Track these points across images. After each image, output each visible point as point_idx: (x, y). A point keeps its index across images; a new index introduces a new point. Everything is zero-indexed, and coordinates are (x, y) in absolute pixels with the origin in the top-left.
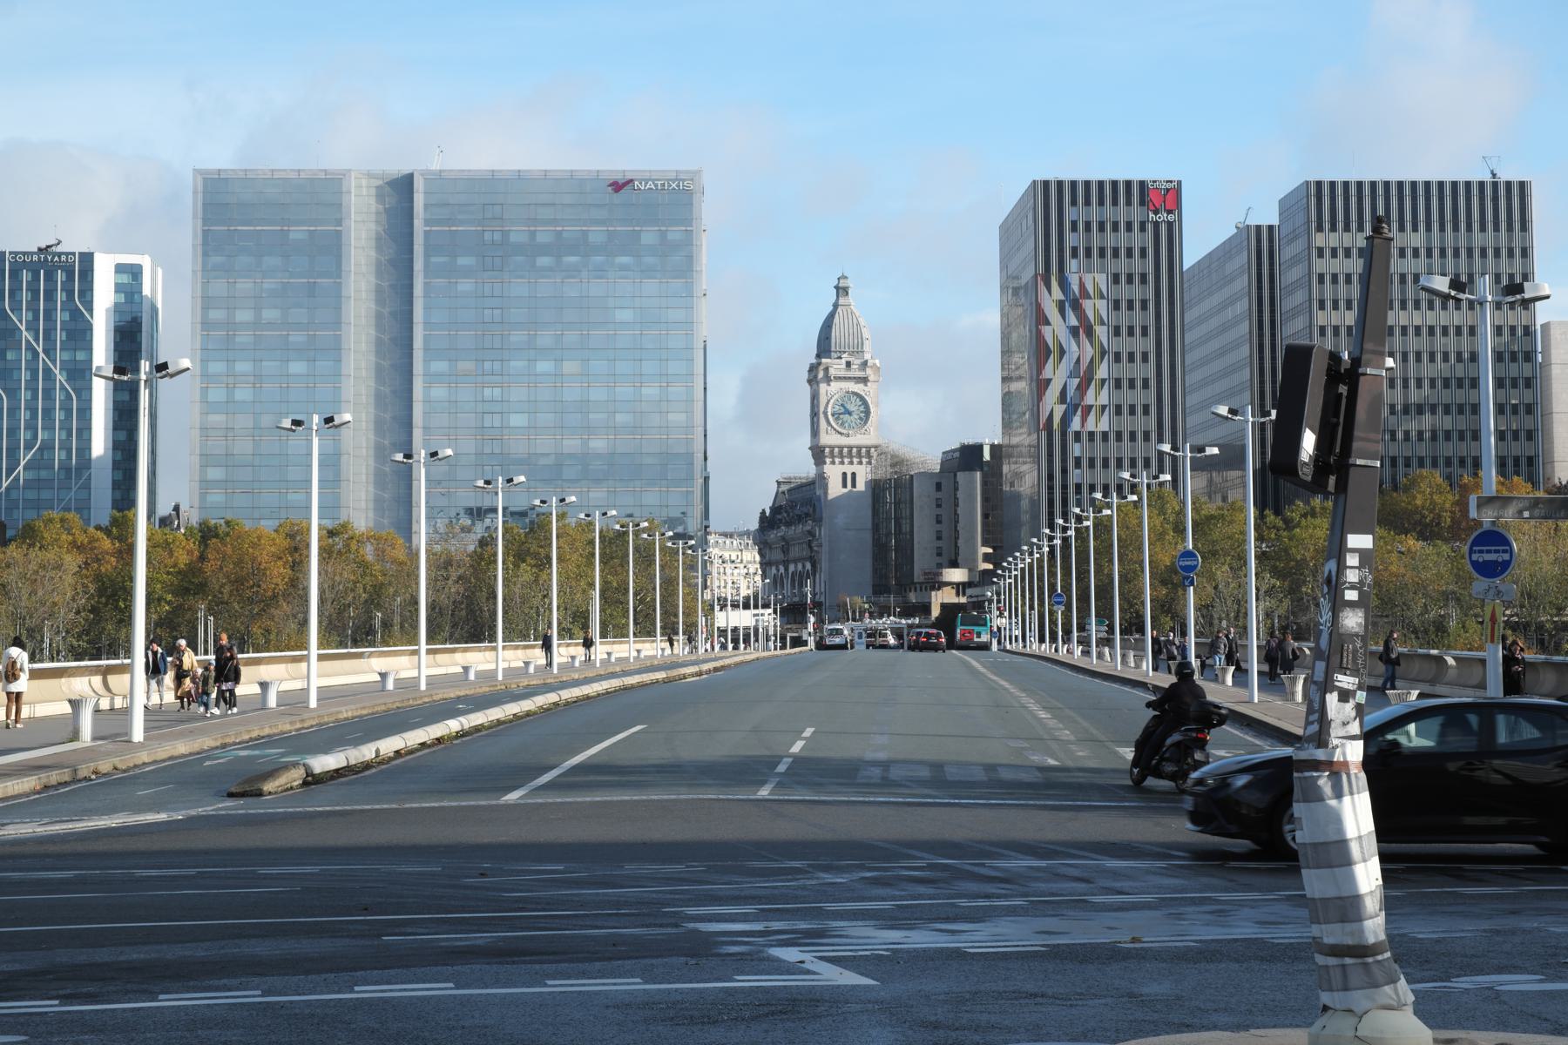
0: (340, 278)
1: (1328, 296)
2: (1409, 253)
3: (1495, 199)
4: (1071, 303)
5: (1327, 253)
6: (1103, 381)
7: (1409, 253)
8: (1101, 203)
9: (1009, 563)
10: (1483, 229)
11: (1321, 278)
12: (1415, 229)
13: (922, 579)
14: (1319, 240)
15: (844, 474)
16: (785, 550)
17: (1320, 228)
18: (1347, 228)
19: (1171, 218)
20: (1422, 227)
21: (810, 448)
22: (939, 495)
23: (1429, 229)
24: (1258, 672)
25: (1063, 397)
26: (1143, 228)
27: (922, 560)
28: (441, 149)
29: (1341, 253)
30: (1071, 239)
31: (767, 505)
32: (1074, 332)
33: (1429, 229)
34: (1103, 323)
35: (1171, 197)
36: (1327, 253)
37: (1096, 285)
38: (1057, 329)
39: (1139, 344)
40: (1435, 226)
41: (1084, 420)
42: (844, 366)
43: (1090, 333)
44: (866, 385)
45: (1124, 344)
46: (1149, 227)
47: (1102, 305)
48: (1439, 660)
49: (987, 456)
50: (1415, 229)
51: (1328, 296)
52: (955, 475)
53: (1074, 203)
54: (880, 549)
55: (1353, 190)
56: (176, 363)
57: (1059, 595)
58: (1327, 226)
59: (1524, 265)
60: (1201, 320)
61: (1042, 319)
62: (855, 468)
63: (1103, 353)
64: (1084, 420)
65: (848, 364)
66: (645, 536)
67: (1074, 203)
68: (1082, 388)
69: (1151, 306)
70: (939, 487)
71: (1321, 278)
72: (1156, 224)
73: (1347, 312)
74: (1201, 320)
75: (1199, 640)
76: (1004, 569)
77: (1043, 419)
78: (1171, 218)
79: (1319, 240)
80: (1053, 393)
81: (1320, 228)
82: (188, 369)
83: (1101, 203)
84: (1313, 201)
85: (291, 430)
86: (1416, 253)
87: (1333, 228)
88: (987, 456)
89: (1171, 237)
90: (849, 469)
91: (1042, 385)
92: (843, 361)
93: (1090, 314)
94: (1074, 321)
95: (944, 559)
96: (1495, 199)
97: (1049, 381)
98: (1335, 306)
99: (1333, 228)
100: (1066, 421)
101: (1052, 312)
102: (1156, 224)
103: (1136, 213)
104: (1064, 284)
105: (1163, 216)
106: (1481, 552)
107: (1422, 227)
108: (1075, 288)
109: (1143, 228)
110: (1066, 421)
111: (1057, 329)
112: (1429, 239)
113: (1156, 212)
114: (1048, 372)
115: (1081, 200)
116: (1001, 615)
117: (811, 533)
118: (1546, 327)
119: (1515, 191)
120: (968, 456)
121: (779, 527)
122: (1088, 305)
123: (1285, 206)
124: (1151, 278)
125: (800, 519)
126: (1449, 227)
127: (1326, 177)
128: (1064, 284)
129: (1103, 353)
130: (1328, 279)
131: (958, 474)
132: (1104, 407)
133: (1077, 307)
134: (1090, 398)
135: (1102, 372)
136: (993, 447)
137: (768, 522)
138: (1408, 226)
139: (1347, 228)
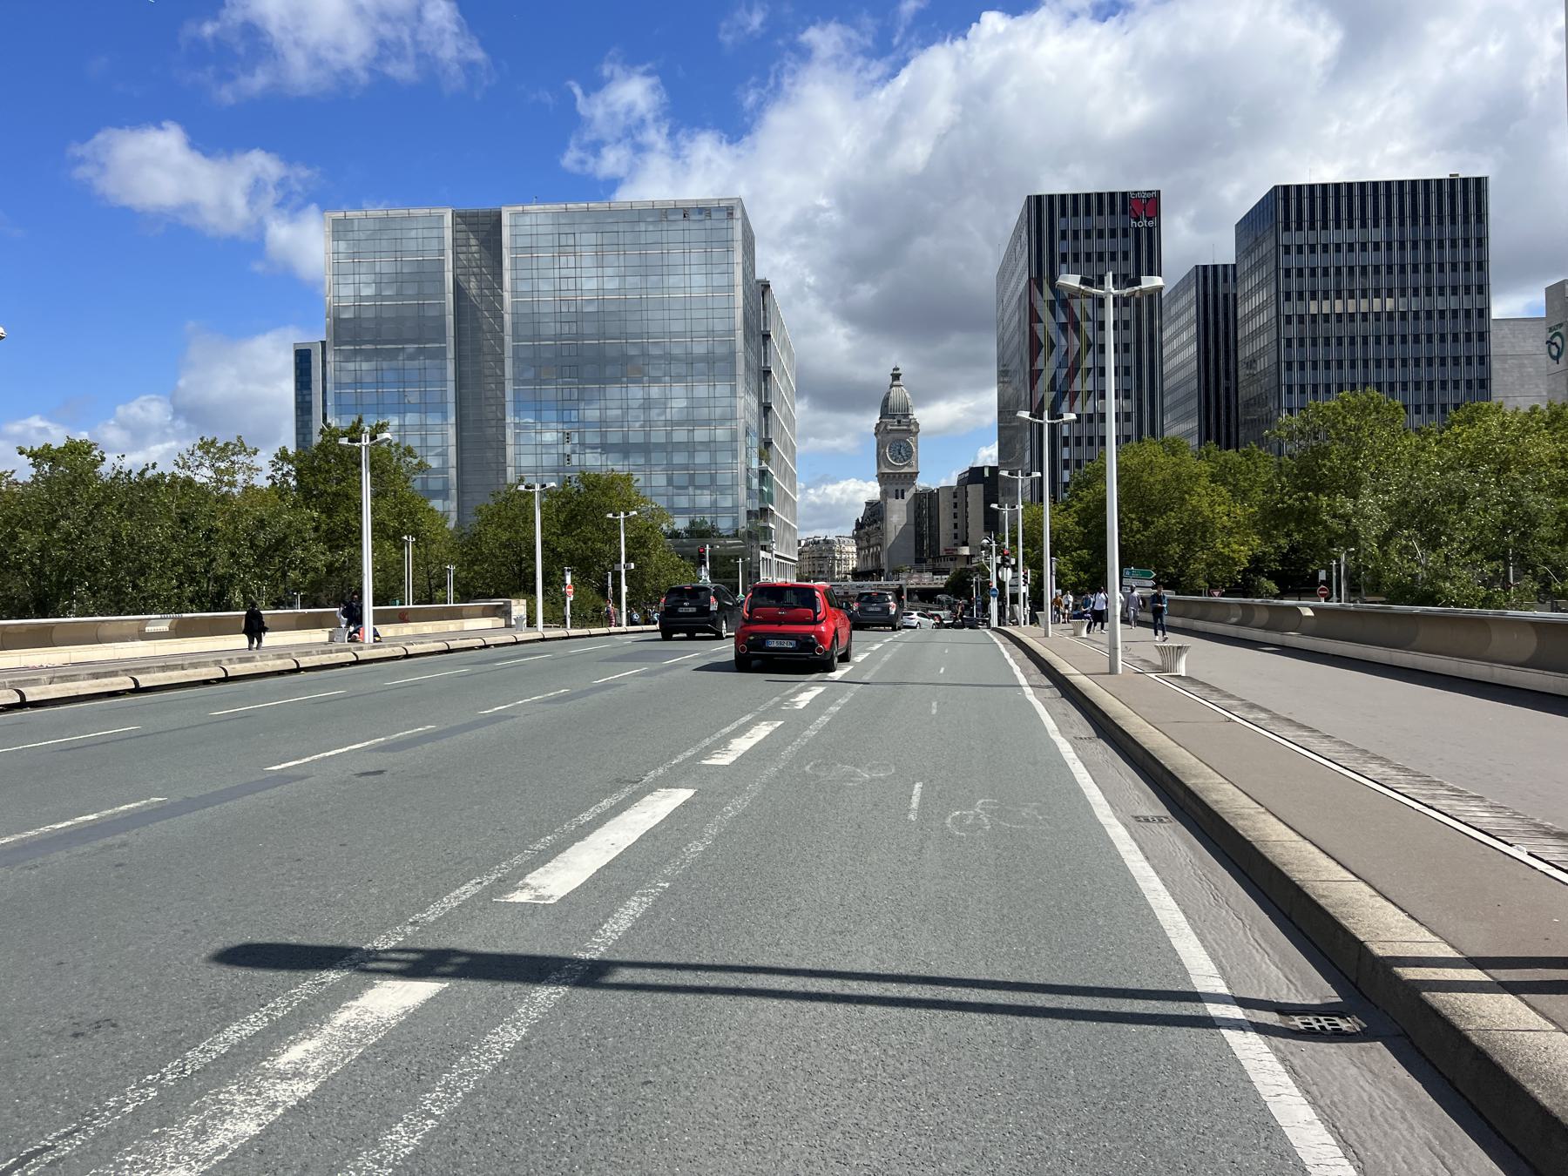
6: (1089, 370)
15: (897, 491)
16: (868, 541)
19: (1151, 223)
20: (1382, 222)
23: (1389, 223)
25: (1052, 387)
27: (945, 541)
30: (1060, 224)
32: (1063, 328)
34: (1088, 319)
43: (1077, 327)
46: (1132, 233)
49: (987, 474)
53: (1063, 214)
54: (919, 537)
59: (1480, 254)
63: (1089, 346)
67: (1063, 214)
68: (1071, 376)
72: (1138, 230)
78: (1151, 223)
83: (1088, 213)
84: (1281, 203)
86: (1377, 246)
88: (987, 474)
91: (1035, 375)
93: (1078, 312)
94: (1063, 319)
101: (1045, 314)
102: (1138, 230)
105: (1144, 223)
107: (1382, 222)
109: (1125, 233)
111: (1048, 325)
113: (1137, 219)
114: (1039, 364)
119: (1472, 187)
120: (975, 475)
125: (875, 522)
126: (1408, 222)
129: (1089, 346)
132: (1089, 392)
134: (1077, 385)
137: (859, 526)
138: (1370, 222)
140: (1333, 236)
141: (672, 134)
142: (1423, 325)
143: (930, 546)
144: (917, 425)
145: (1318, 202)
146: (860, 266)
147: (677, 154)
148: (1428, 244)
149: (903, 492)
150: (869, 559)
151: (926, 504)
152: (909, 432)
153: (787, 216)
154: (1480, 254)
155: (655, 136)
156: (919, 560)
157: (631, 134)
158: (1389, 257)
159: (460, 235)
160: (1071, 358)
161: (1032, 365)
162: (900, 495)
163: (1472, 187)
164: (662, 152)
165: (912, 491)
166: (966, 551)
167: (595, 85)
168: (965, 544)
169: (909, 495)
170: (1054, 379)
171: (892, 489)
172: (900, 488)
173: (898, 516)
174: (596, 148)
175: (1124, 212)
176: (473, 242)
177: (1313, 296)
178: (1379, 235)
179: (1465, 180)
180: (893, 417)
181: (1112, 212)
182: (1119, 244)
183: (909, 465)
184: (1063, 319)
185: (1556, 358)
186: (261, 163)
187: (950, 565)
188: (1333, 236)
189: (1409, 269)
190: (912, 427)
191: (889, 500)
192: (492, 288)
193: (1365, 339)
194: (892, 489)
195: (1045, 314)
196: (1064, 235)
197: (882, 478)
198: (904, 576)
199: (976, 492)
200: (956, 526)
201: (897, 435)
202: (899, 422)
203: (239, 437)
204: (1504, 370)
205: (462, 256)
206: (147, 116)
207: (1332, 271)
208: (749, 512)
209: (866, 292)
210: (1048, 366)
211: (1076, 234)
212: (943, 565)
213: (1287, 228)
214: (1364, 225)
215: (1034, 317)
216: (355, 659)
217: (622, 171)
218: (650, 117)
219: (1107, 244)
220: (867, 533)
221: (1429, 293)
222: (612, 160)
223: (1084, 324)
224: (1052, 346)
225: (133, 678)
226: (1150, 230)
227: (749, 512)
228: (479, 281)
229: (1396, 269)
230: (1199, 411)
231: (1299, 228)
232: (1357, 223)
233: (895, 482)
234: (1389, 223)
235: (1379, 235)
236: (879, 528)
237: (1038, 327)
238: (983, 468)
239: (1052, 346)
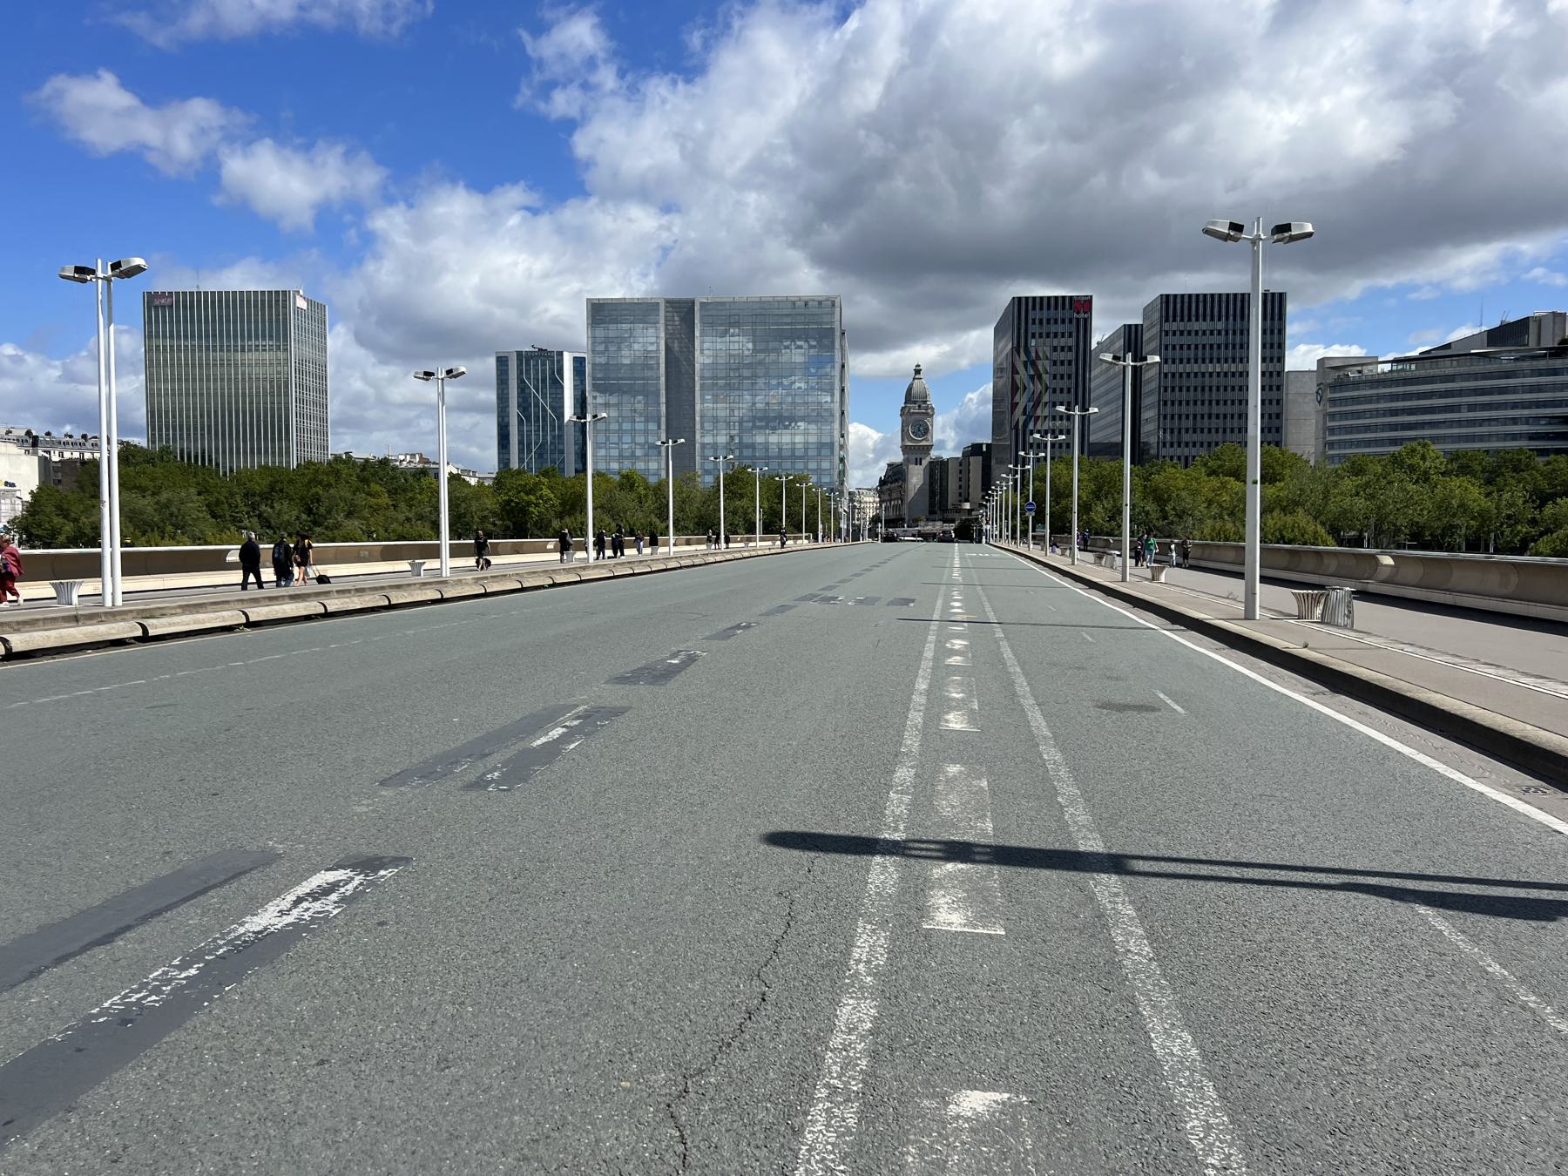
4: (1031, 363)
6: (1046, 403)
8: (1049, 308)
9: (993, 491)
16: (890, 495)
17: (1167, 320)
18: (1182, 320)
19: (1086, 316)
23: (1227, 319)
24: (1261, 577)
25: (1024, 413)
26: (1071, 322)
27: (952, 498)
30: (1032, 328)
31: (883, 475)
32: (1032, 377)
34: (1047, 373)
36: (1170, 333)
37: (1044, 352)
38: (1023, 376)
39: (1065, 383)
41: (1035, 424)
43: (1040, 378)
45: (1059, 384)
46: (1074, 322)
47: (1047, 363)
48: (1108, 540)
49: (984, 449)
50: (1219, 320)
54: (932, 493)
56: (129, 262)
57: (1031, 504)
59: (1279, 338)
60: (1097, 377)
61: (1015, 371)
63: (1047, 389)
64: (1035, 424)
66: (750, 470)
67: (1034, 308)
68: (1035, 407)
69: (1073, 363)
72: (1078, 320)
74: (1097, 377)
75: (1366, 544)
76: (993, 491)
77: (1014, 424)
78: (1086, 316)
79: (1166, 326)
80: (1019, 410)
81: (1167, 320)
82: (463, 373)
83: (1049, 308)
85: (73, 279)
87: (1174, 320)
88: (984, 449)
89: (1085, 328)
91: (1014, 406)
93: (1040, 368)
94: (1032, 373)
95: (962, 498)
97: (1017, 404)
98: (1174, 362)
100: (1026, 424)
101: (1021, 368)
102: (1078, 320)
103: (1068, 313)
104: (1027, 352)
105: (1082, 315)
108: (1033, 354)
109: (1071, 322)
110: (1026, 424)
111: (1023, 376)
112: (1227, 325)
113: (1078, 313)
114: (1017, 399)
115: (1038, 306)
116: (987, 523)
117: (901, 486)
119: (1277, 298)
120: (975, 449)
122: (1040, 364)
123: (1147, 311)
125: (897, 481)
126: (1238, 318)
128: (1027, 352)
129: (1047, 389)
132: (1046, 417)
133: (1034, 364)
134: (1039, 412)
135: (1046, 398)
136: (987, 445)
137: (882, 483)
140: (1195, 326)
141: (622, 74)
143: (940, 502)
144: (933, 409)
146: (832, 206)
147: (633, 92)
149: (921, 460)
150: (891, 510)
151: (938, 469)
152: (927, 414)
153: (746, 156)
154: (1279, 338)
155: (607, 77)
156: (932, 512)
157: (582, 74)
158: (1227, 339)
159: (668, 314)
160: (1036, 396)
161: (1012, 399)
162: (918, 462)
163: (1277, 298)
164: (613, 93)
165: (928, 459)
166: (967, 506)
167: (541, 29)
168: (967, 501)
169: (925, 462)
170: (1025, 408)
171: (913, 457)
172: (919, 456)
173: (916, 478)
174: (547, 89)
175: (1071, 308)
176: (676, 318)
177: (1181, 361)
178: (1220, 325)
179: (1273, 294)
180: (915, 402)
181: (1063, 308)
182: (1066, 328)
183: (927, 440)
184: (1032, 373)
185: (1319, 402)
186: (201, 110)
187: (956, 516)
188: (1195, 326)
189: (1238, 346)
190: (929, 411)
191: (910, 466)
192: (688, 347)
193: (1211, 388)
194: (913, 457)
195: (1021, 368)
197: (905, 449)
198: (922, 523)
201: (917, 417)
202: (919, 406)
204: (1305, 403)
205: (670, 327)
206: (84, 67)
207: (1193, 347)
209: (831, 235)
210: (1022, 400)
211: (1041, 321)
212: (950, 516)
215: (1015, 371)
216: (323, 611)
217: (573, 112)
218: (601, 55)
219: (1060, 328)
220: (889, 489)
222: (562, 103)
223: (1044, 376)
224: (1025, 388)
225: (140, 624)
226: (1085, 320)
228: (680, 343)
231: (1174, 320)
232: (1208, 318)
233: (915, 452)
234: (1227, 319)
235: (1220, 325)
236: (901, 486)
237: (1017, 377)
238: (982, 444)
239: (1025, 388)
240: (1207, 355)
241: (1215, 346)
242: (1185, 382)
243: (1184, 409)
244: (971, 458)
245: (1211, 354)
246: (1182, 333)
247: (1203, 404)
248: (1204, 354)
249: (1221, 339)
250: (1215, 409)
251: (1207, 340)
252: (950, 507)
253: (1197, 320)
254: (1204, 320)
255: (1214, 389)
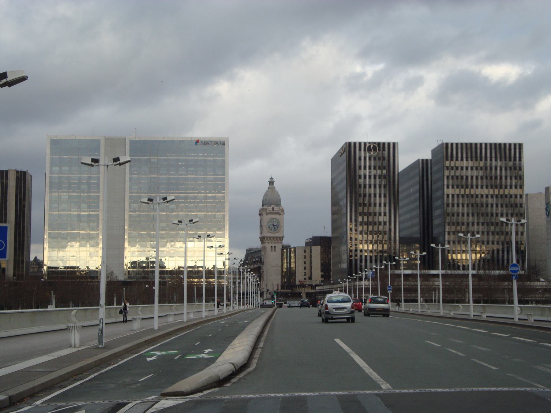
0: (100, 175)
1: (508, 183)
2: (479, 168)
3: (510, 150)
5: (450, 168)
7: (479, 168)
10: (510, 160)
11: (448, 177)
12: (481, 160)
13: (299, 284)
14: (447, 163)
15: (272, 247)
18: (457, 160)
20: (484, 159)
21: (260, 238)
22: (305, 254)
23: (486, 160)
28: (136, 130)
29: (455, 168)
33: (486, 160)
35: (394, 146)
36: (450, 168)
40: (489, 159)
42: (272, 209)
44: (280, 216)
50: (481, 160)
51: (508, 183)
52: (311, 247)
53: (360, 150)
55: (459, 146)
58: (450, 159)
62: (276, 245)
65: (273, 208)
67: (360, 150)
70: (305, 251)
71: (448, 177)
73: (476, 190)
79: (447, 163)
81: (447, 160)
84: (445, 150)
86: (481, 168)
90: (273, 245)
92: (271, 208)
96: (510, 150)
99: (452, 160)
106: (512, 268)
107: (484, 159)
115: (362, 149)
118: (527, 195)
120: (316, 241)
121: (257, 263)
123: (434, 152)
124: (387, 177)
127: (450, 141)
130: (450, 177)
131: (312, 247)
138: (479, 159)
139: (457, 160)
140: (464, 163)
142: (490, 209)
145: (459, 150)
148: (491, 178)
158: (486, 173)
178: (482, 164)
188: (464, 163)
196: (360, 177)
199: (317, 250)
200: (305, 268)
203: (87, 267)
208: (161, 259)
213: (447, 160)
214: (476, 160)
221: (501, 187)
227: (161, 259)
229: (489, 178)
230: (432, 210)
232: (474, 159)
235: (482, 164)
240: (504, 183)
241: (450, 177)
242: (460, 200)
243: (368, 181)
244: (313, 248)
245: (472, 183)
246: (457, 168)
247: (473, 215)
248: (496, 182)
249: (482, 173)
250: (481, 219)
251: (474, 173)
252: (298, 283)
253: (467, 160)
254: (472, 160)
255: (480, 205)
